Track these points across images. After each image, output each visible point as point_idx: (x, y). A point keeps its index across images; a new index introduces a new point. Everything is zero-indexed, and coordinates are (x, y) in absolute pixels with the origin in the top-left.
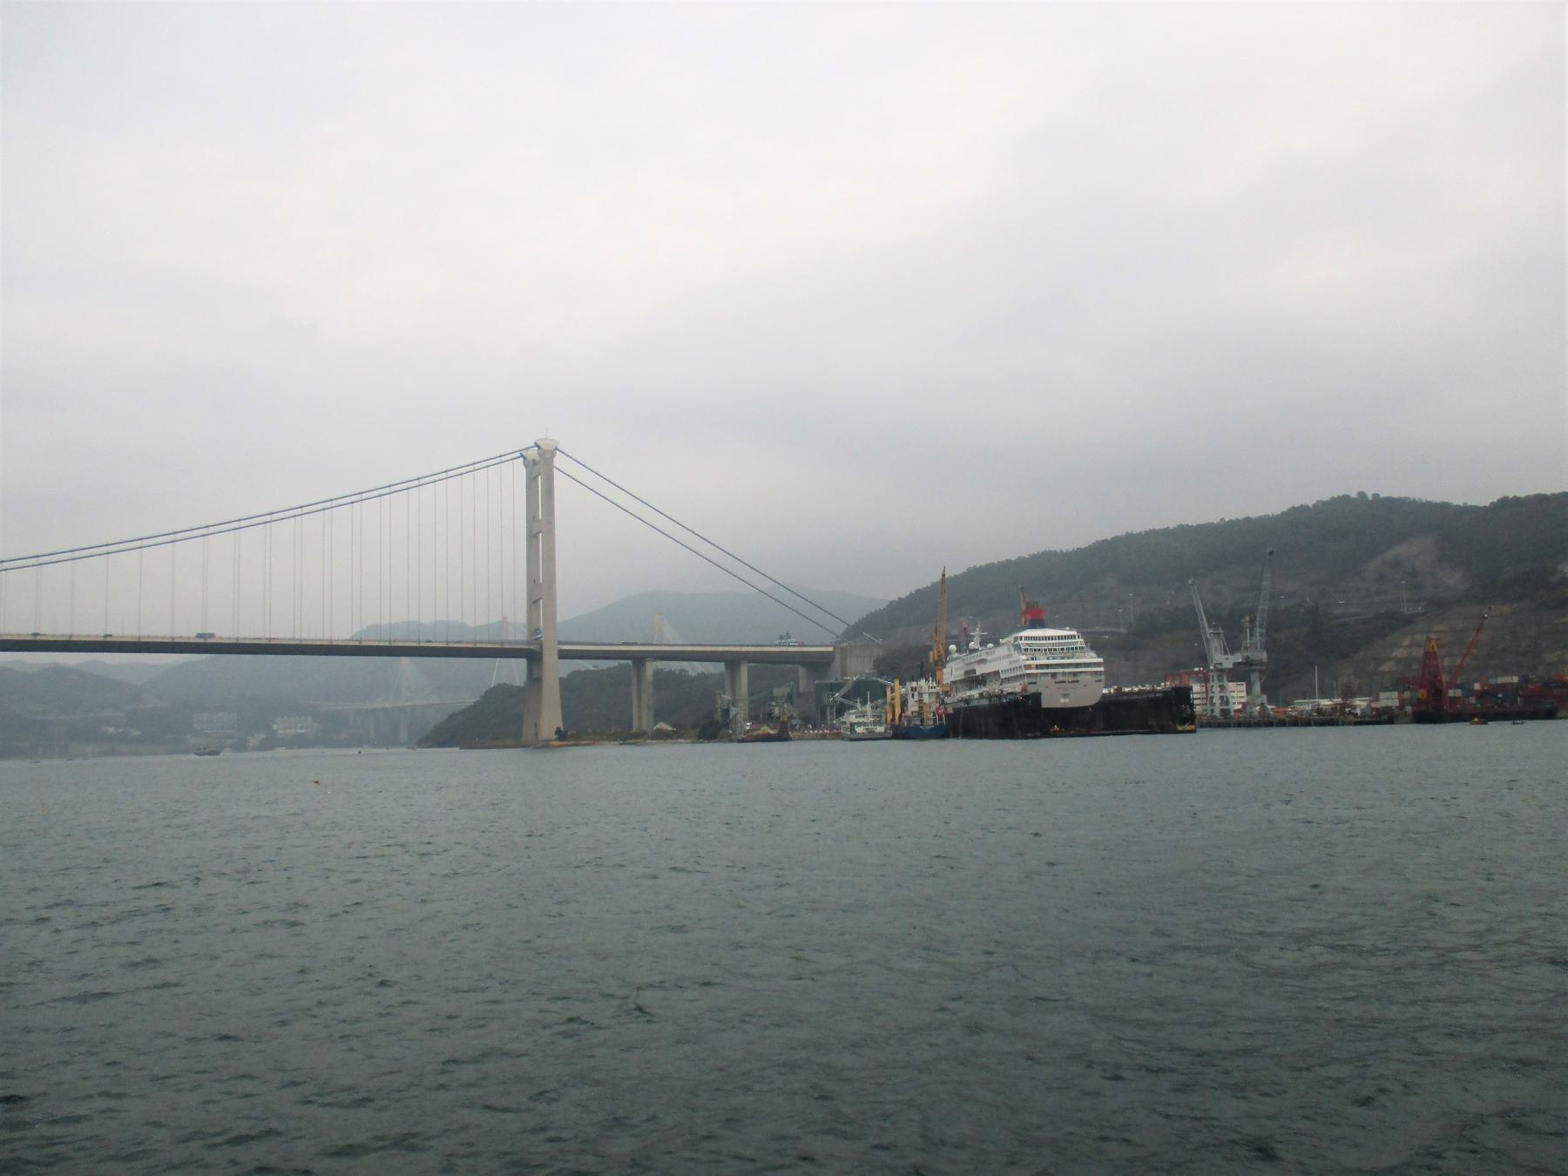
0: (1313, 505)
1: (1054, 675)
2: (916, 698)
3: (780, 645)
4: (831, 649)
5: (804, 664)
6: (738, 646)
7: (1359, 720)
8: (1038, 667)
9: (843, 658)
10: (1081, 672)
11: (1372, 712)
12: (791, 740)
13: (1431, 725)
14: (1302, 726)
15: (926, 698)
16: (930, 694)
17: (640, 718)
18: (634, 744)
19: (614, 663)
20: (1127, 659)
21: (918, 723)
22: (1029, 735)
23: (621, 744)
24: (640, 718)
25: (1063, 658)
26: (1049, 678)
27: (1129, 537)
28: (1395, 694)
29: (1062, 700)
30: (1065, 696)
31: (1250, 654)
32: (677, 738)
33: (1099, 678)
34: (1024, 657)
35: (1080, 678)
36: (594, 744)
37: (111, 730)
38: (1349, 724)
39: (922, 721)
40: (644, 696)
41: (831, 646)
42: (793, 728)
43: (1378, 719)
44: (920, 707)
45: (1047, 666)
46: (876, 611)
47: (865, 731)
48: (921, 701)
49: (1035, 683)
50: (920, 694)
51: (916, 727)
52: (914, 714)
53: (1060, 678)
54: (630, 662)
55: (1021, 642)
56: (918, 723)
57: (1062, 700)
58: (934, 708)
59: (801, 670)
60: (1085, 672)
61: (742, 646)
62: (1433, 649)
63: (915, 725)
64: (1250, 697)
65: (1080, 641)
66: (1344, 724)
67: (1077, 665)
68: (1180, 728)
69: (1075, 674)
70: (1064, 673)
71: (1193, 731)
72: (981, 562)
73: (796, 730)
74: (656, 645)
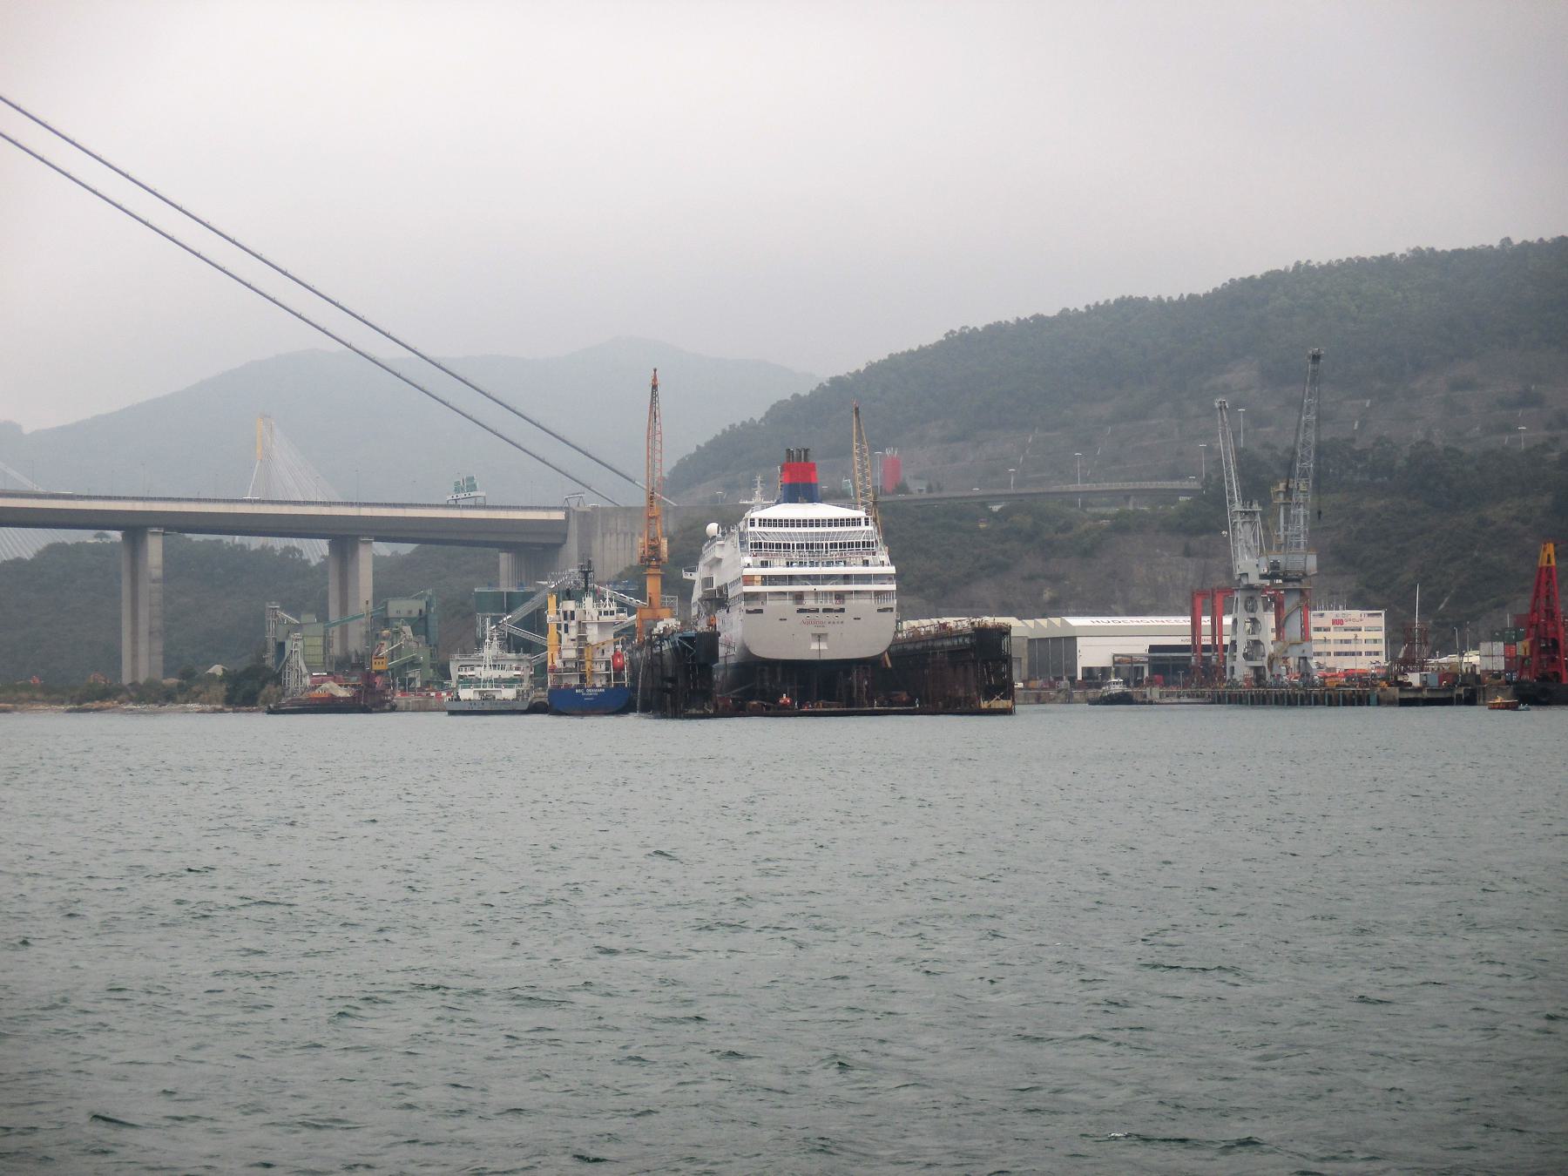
0: (1261, 276)
1: (799, 597)
2: (573, 633)
3: (456, 507)
4: (559, 516)
5: (506, 547)
6: (352, 504)
7: (1412, 695)
8: (767, 580)
9: (586, 537)
10: (851, 592)
11: (1440, 682)
12: (393, 709)
13: (706, 720)
14: (1344, 704)
15: (593, 635)
16: (602, 625)
17: (135, 656)
18: (97, 710)
19: (88, 537)
20: (1188, 553)
21: (575, 682)
22: (694, 711)
23: (69, 711)
24: (135, 656)
25: (829, 564)
26: (789, 603)
27: (1304, 273)
28: (1499, 647)
29: (815, 646)
30: (819, 637)
31: (1281, 559)
32: (187, 702)
33: (886, 605)
34: (748, 560)
35: (850, 603)
36: (15, 709)
37: (1104, 499)
38: (1391, 703)
39: (582, 678)
40: (143, 613)
41: (560, 509)
42: (407, 686)
43: (1448, 695)
44: (580, 651)
45: (791, 579)
46: (743, 424)
47: (477, 697)
48: (582, 639)
49: (760, 611)
50: (582, 626)
51: (570, 690)
52: (568, 665)
53: (809, 603)
54: (116, 535)
55: (750, 529)
56: (575, 682)
57: (815, 646)
58: (609, 654)
59: (505, 560)
60: (857, 592)
61: (361, 505)
62: (1549, 561)
63: (567, 686)
64: (1280, 644)
65: (868, 530)
66: (1379, 702)
67: (846, 578)
68: (984, 705)
69: (840, 596)
70: (816, 593)
71: (1007, 712)
72: (1256, 265)
73: (412, 690)
74: (250, 501)
